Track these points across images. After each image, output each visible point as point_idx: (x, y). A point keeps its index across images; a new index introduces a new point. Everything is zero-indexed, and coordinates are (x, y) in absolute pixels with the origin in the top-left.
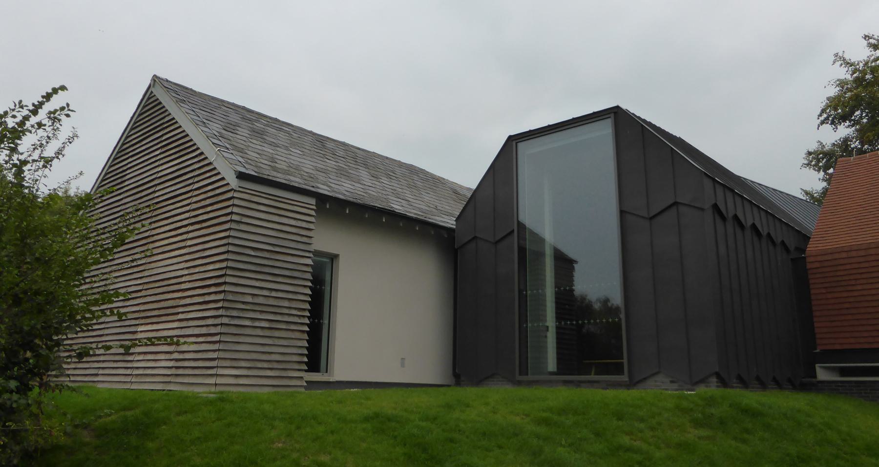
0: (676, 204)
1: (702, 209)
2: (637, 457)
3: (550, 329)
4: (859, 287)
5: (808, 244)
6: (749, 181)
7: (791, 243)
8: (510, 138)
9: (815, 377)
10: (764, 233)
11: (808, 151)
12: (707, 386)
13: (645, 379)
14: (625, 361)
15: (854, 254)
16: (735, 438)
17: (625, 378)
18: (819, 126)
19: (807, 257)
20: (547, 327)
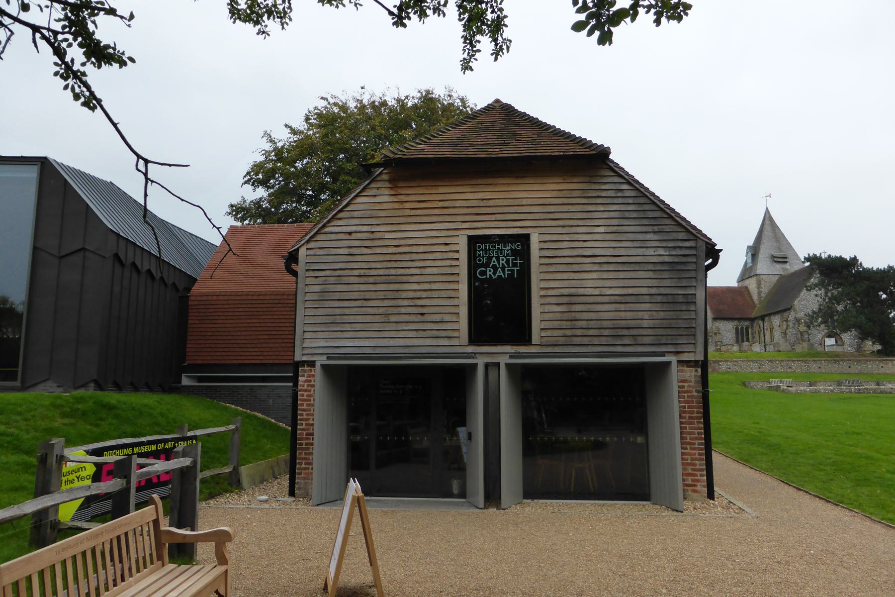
0: (83, 249)
1: (104, 257)
2: (9, 439)
4: (220, 322)
5: (193, 287)
6: (170, 225)
7: (181, 287)
12: (86, 390)
13: (36, 384)
15: (221, 298)
16: (91, 424)
17: (18, 384)
18: (242, 185)
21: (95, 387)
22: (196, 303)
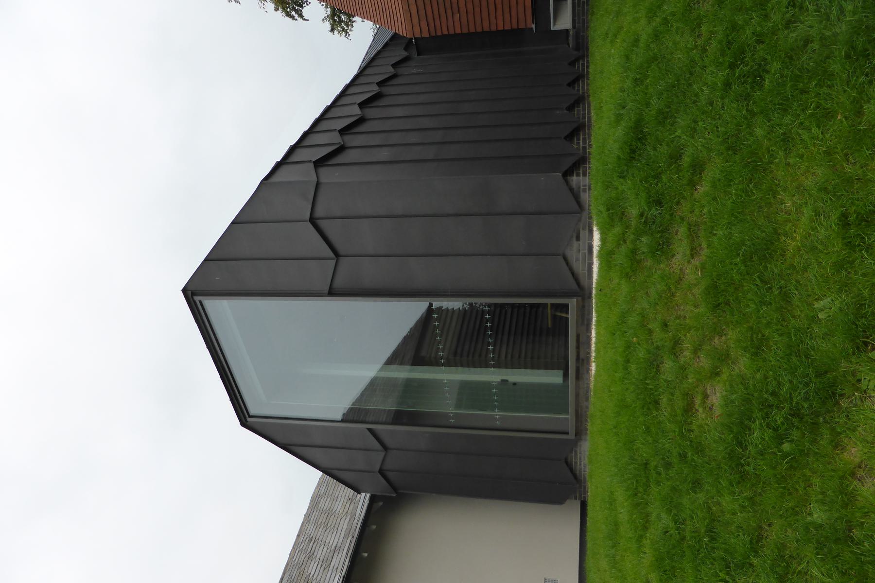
0: (313, 220)
3: (505, 378)
7: (400, 53)
8: (244, 424)
9: (567, 31)
10: (375, 89)
11: (331, 31)
14: (550, 301)
16: (693, 184)
19: (414, 36)
20: (502, 381)
21: (578, 175)
22: (424, 24)
